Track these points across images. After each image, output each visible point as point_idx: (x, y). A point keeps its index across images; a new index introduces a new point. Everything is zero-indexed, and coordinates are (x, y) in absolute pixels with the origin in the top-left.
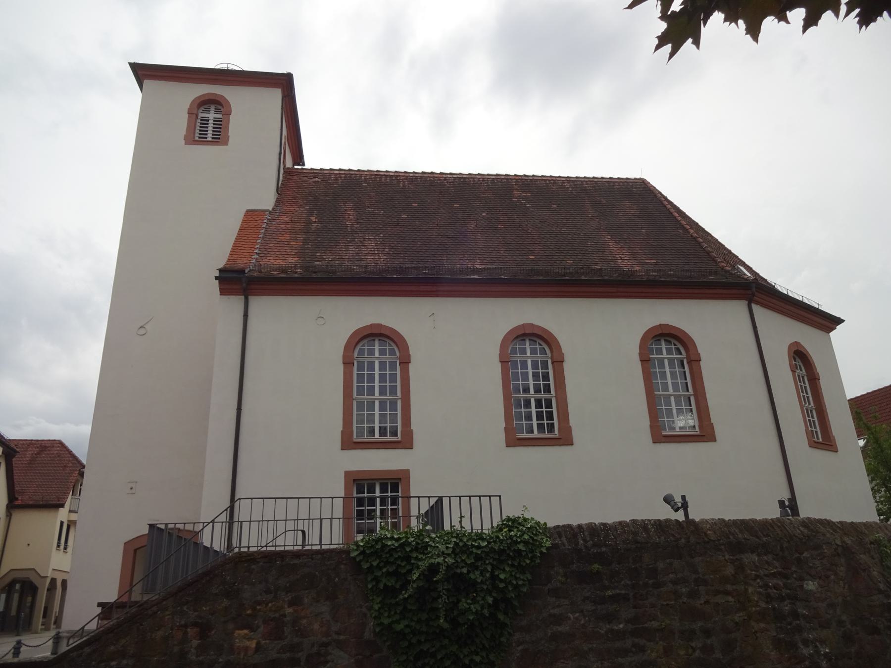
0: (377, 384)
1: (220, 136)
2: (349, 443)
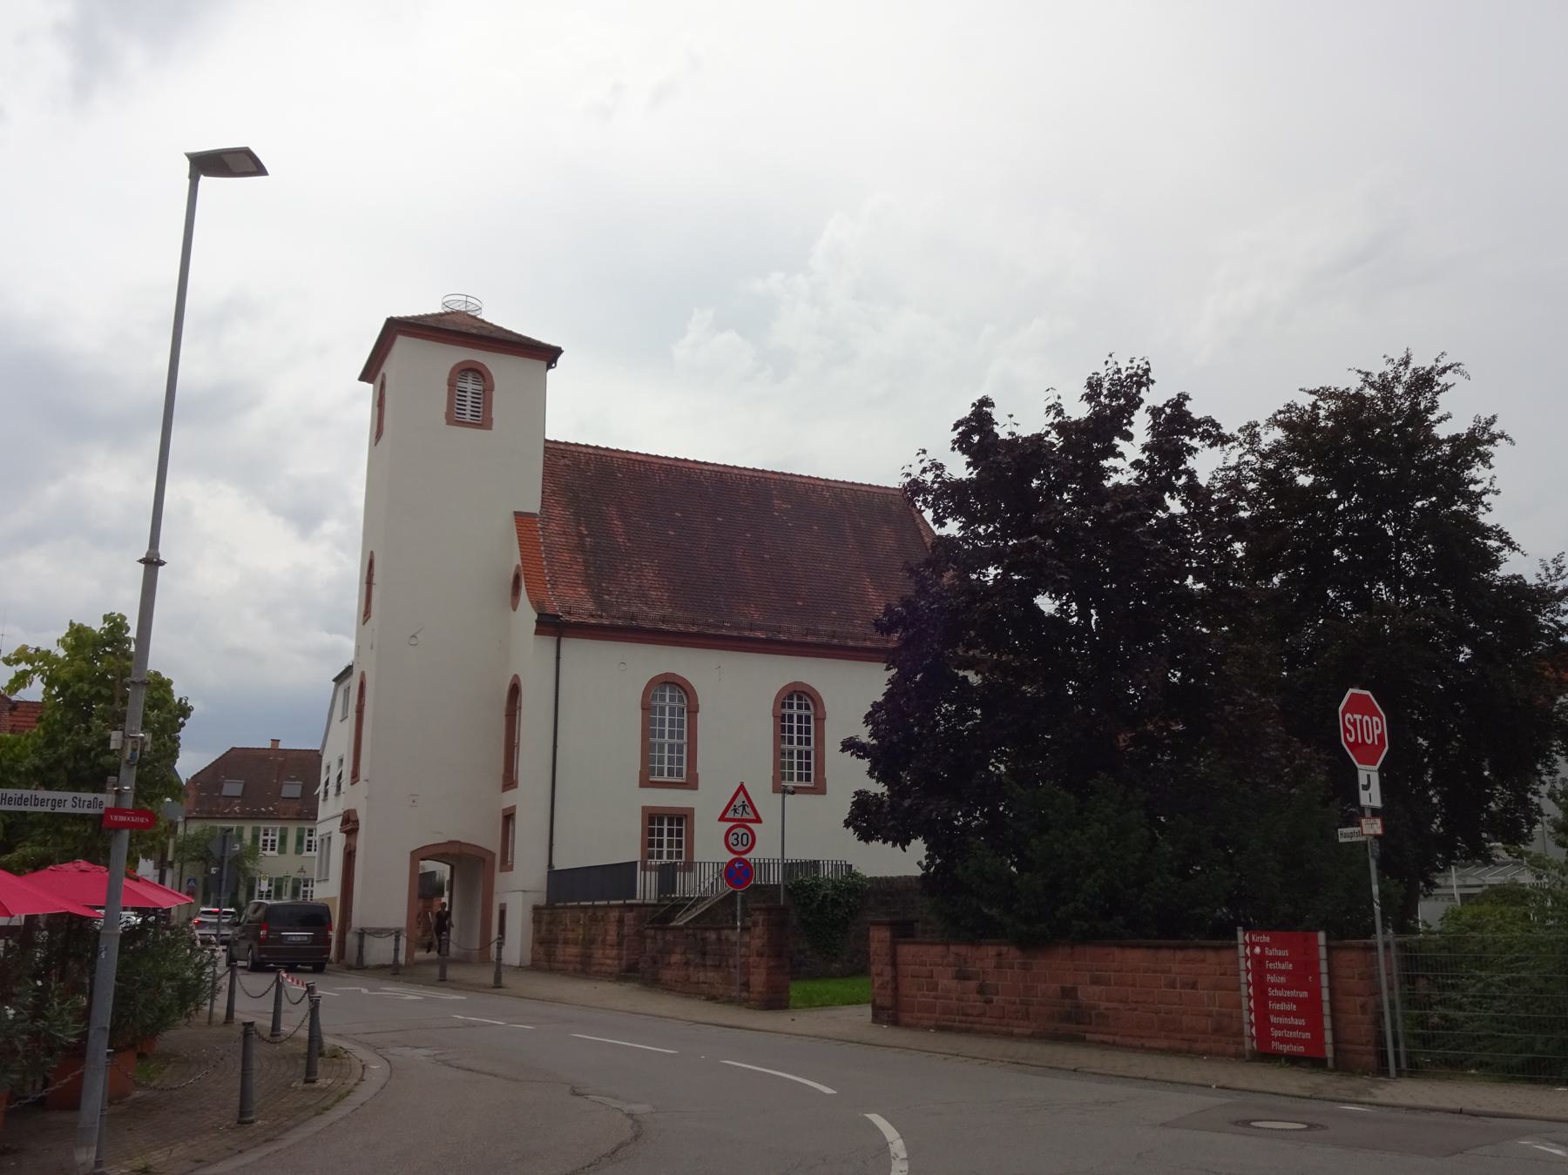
0: (667, 728)
1: (483, 421)
2: (645, 782)
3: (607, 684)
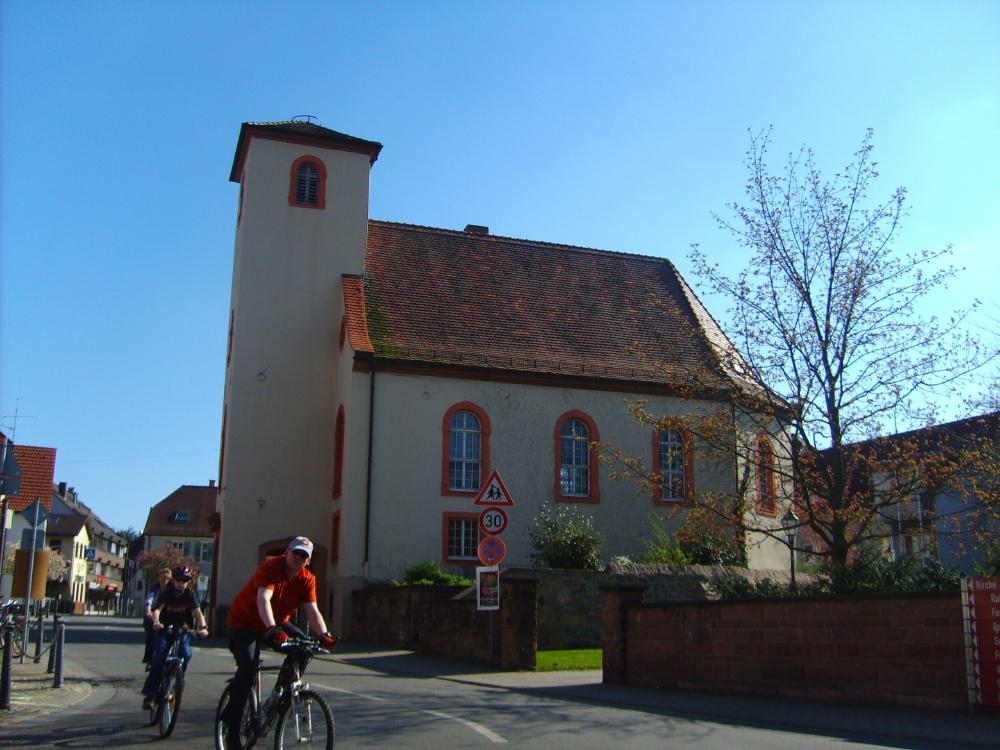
3: (415, 410)
